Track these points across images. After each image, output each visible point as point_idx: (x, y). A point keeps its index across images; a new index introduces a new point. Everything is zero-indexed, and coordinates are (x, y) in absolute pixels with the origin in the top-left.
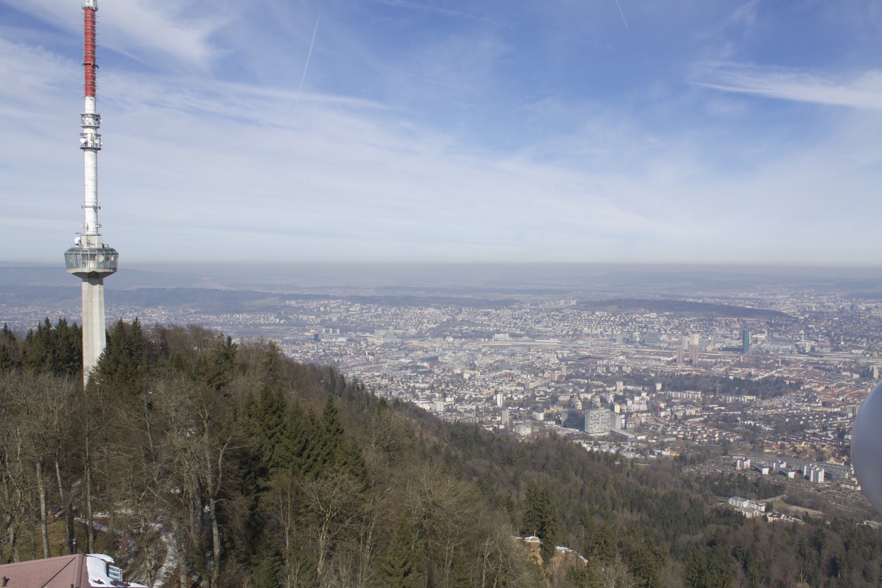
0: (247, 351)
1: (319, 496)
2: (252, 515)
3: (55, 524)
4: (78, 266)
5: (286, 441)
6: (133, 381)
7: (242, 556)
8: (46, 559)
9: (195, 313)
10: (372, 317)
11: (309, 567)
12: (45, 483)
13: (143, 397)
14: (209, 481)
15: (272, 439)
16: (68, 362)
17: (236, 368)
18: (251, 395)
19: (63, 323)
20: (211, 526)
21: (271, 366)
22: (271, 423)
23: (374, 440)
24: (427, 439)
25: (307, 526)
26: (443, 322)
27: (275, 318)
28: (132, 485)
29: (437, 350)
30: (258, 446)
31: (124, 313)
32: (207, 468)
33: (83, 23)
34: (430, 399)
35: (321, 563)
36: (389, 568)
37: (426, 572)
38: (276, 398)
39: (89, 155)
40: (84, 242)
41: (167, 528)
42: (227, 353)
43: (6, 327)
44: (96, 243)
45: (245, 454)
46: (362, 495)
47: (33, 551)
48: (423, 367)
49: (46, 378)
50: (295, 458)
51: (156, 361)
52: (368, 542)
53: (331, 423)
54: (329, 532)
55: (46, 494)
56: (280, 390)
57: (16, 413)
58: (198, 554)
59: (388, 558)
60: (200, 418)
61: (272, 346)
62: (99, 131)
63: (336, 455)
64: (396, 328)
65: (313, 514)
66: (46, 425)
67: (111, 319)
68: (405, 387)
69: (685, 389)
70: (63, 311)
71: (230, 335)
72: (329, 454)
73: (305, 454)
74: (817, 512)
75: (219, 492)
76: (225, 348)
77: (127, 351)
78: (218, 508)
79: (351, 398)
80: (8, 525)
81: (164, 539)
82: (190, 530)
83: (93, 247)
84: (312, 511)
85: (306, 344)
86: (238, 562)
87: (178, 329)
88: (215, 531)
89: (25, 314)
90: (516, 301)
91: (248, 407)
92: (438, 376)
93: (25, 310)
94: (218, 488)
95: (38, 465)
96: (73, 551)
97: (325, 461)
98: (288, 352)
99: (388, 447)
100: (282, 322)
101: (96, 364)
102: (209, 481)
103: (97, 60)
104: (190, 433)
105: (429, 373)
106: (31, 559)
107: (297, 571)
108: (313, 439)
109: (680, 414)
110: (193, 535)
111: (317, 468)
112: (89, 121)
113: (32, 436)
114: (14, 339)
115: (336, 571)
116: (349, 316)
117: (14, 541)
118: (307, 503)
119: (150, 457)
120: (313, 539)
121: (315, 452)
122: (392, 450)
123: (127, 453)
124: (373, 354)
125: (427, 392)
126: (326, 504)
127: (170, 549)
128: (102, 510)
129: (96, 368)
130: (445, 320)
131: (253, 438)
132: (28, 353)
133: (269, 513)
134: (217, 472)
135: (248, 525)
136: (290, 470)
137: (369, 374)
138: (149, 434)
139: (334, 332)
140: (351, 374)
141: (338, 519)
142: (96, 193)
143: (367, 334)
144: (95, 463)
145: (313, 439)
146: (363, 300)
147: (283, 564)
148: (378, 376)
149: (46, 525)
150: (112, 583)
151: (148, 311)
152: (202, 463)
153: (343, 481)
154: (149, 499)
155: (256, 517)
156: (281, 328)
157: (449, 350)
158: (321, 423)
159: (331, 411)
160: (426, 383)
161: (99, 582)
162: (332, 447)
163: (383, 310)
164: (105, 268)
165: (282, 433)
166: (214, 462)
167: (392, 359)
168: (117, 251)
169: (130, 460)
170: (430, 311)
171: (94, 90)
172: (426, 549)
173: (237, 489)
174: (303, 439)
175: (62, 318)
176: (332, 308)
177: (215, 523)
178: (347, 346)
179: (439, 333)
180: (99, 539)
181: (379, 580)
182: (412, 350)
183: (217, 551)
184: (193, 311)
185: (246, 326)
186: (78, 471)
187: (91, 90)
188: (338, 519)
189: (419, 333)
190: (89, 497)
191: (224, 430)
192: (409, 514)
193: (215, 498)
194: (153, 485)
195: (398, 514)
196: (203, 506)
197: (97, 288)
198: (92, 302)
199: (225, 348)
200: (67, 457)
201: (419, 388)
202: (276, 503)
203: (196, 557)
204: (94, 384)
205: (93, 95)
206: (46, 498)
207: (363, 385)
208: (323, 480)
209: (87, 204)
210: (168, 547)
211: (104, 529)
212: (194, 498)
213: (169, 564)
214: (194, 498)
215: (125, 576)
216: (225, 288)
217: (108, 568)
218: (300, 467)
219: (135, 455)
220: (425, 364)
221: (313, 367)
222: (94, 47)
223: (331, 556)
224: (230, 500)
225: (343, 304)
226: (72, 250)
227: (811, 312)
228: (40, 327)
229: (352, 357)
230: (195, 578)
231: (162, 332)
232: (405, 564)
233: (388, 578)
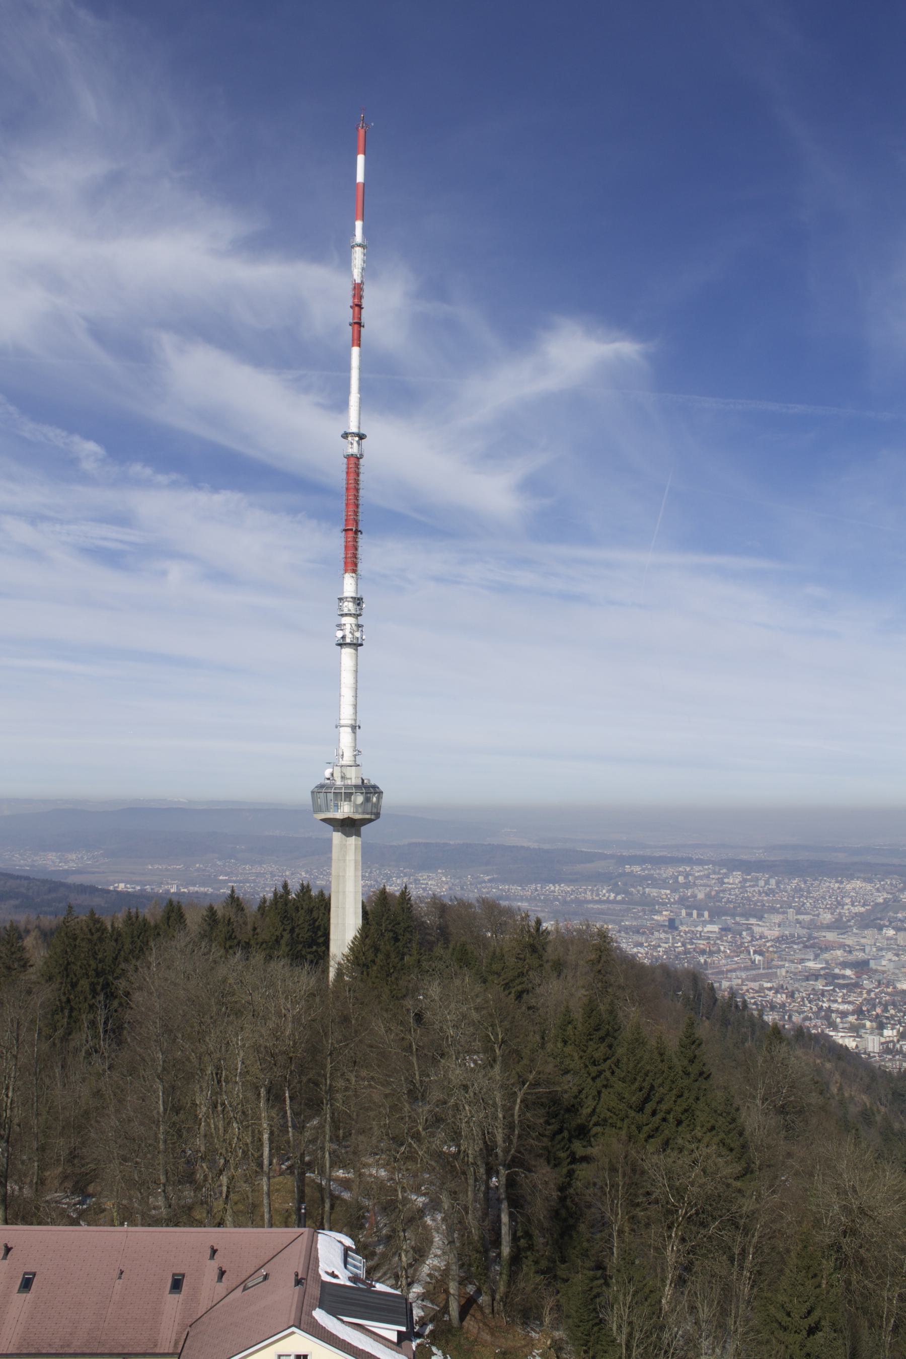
0: (565, 941)
1: (669, 1179)
2: (563, 1199)
3: (281, 1178)
4: (328, 810)
5: (619, 1086)
6: (397, 979)
7: (544, 1264)
8: (266, 1230)
9: (490, 881)
10: (760, 893)
11: (647, 1296)
12: (270, 1118)
13: (409, 1003)
14: (499, 1138)
15: (598, 1080)
16: (310, 946)
17: (547, 966)
18: (568, 1010)
19: (305, 890)
20: (500, 1210)
21: (599, 967)
22: (597, 1055)
23: (761, 1092)
24: (851, 1098)
25: (647, 1225)
26: (877, 904)
27: (609, 891)
28: (387, 1135)
29: (867, 949)
30: (575, 1090)
31: (389, 878)
32: (496, 1118)
33: (344, 476)
34: (855, 1030)
35: (668, 1290)
36: (781, 1316)
37: (847, 1333)
38: (605, 1016)
39: (347, 652)
40: (337, 776)
41: (435, 1205)
42: (535, 942)
43: (233, 891)
44: (353, 776)
45: (555, 1101)
46: (738, 1184)
47: (250, 1215)
48: (844, 977)
49: (279, 967)
50: (632, 1113)
51: (431, 950)
52: (747, 1264)
53: (692, 1061)
54: (683, 1240)
55: (272, 1133)
56: (612, 1003)
57: (238, 1013)
58: (477, 1252)
59: (781, 1298)
60: (490, 1041)
61: (603, 935)
62: (361, 620)
63: (698, 1113)
64: (798, 913)
65: (658, 1207)
66: (276, 1034)
67: (371, 886)
68: (815, 1009)
70: (307, 872)
71: (541, 915)
72: (686, 1111)
73: (649, 1107)
75: (514, 1157)
76: (531, 935)
77: (391, 934)
78: (511, 1183)
79: (725, 1022)
80: (221, 1172)
81: (428, 1220)
82: (467, 1213)
83: (349, 782)
84: (657, 1202)
85: (656, 933)
86: (537, 1272)
87: (464, 905)
88: (505, 1218)
89: (258, 875)
91: (563, 1027)
92: (869, 992)
93: (257, 869)
94: (513, 1151)
95: (263, 1091)
96: (301, 1223)
97: (679, 1123)
98: (627, 945)
99: (783, 1106)
100: (619, 898)
101: (346, 951)
102: (499, 1138)
103: (360, 524)
104: (475, 1062)
105: (853, 987)
106: (246, 1226)
107: (629, 1299)
108: (661, 1085)
110: (471, 1220)
111: (666, 1132)
112: (349, 606)
113: (256, 1048)
114: (243, 909)
115: (693, 1309)
116: (723, 891)
117: (227, 1197)
118: (649, 1188)
119: (416, 1095)
120: (657, 1249)
121: (664, 1107)
122: (789, 1112)
123: (383, 1085)
124: (761, 953)
125: (852, 1019)
126: (679, 1193)
127: (437, 1239)
128: (344, 1167)
129: (347, 957)
130: (881, 900)
131: (569, 1077)
132: (258, 930)
133: (588, 1198)
134: (511, 1127)
135: (555, 1215)
136: (624, 1132)
137: (755, 985)
138: (414, 1060)
139: (700, 915)
140: (725, 984)
141: (698, 1220)
142: (355, 706)
143: (753, 921)
144: (339, 1096)
145: (661, 1085)
146: (747, 867)
147: (607, 1284)
148: (770, 989)
149: (269, 1178)
150: (350, 1279)
151: (423, 876)
152: (490, 1110)
153: (708, 1157)
154: (410, 1157)
155: (568, 1202)
156: (618, 907)
157: (889, 949)
158: (675, 1060)
159: (692, 1042)
160: (849, 1003)
161: (333, 1275)
162: (691, 1101)
163: (778, 883)
164: (364, 813)
165: (613, 1073)
166: (508, 1110)
167: (792, 962)
168: (382, 788)
169: (386, 1096)
171: (356, 565)
172: (848, 1290)
173: (540, 1156)
174: (646, 1085)
175: (305, 883)
176: (696, 878)
177: (504, 1205)
178: (720, 939)
179: (871, 921)
180: (338, 1209)
181: (765, 1336)
182: (827, 948)
183: (506, 1250)
184: (487, 878)
185: (565, 902)
186: (314, 1105)
187: (352, 564)
188: (698, 1220)
189: (837, 920)
190: (327, 1145)
191: (525, 1061)
192: (817, 1223)
193: (508, 1167)
194: (417, 1137)
195: (800, 1223)
196: (489, 1177)
197: (352, 840)
198: (345, 860)
199: (531, 935)
200: (301, 1083)
201: (837, 1011)
202: (599, 1184)
203: (475, 1255)
204: (343, 979)
205: (354, 571)
206: (271, 1141)
207: (745, 1002)
208: (675, 1153)
209: (343, 722)
210: (435, 1234)
211: (346, 1195)
212: (475, 1164)
213: (433, 1263)
214: (475, 1164)
215: (369, 1272)
216: (534, 845)
217: (346, 1256)
218: (639, 1129)
219: (393, 1090)
220: (848, 972)
221: (665, 970)
222: (357, 506)
223: (685, 1282)
224: (530, 1171)
225: (714, 873)
226: (322, 786)
228: (275, 894)
229: (727, 957)
230: (471, 1289)
231: (441, 907)
232: (809, 1313)
233: (780, 1334)
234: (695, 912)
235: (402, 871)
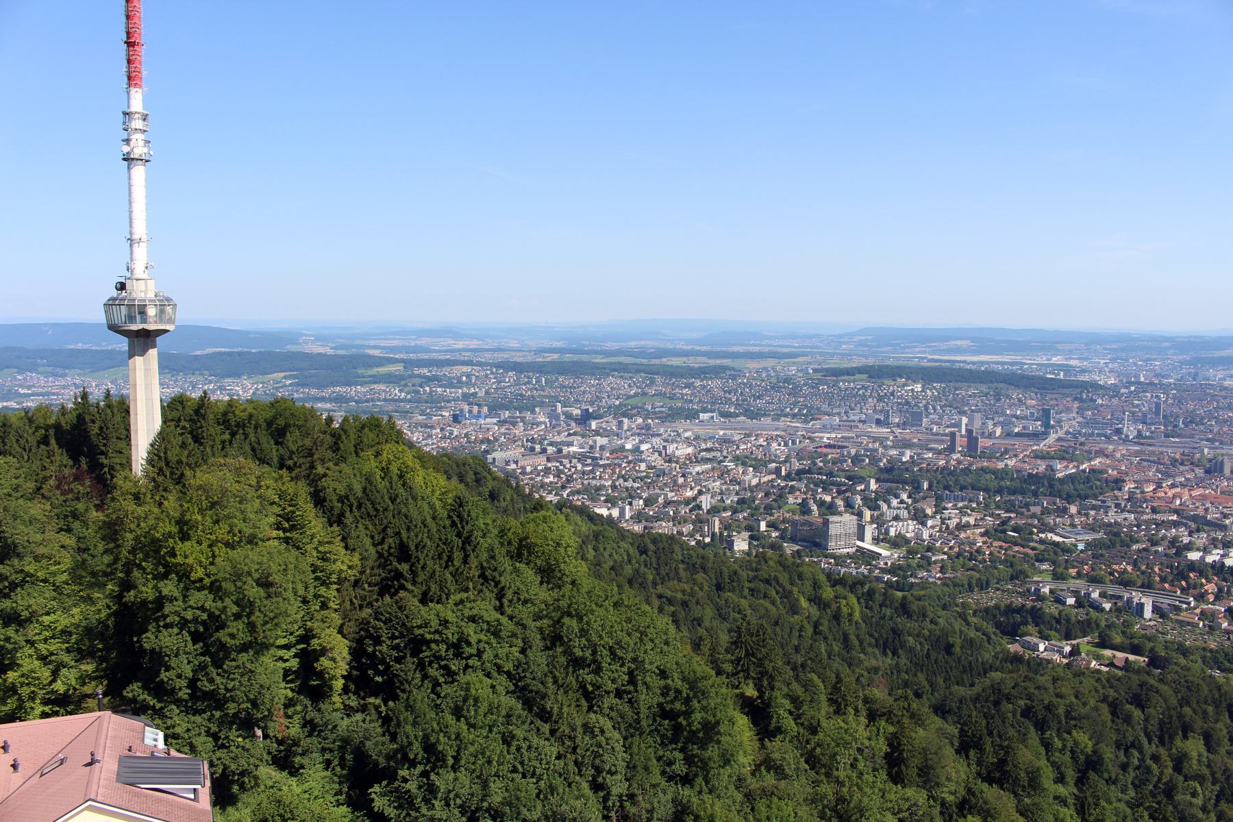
9: (291, 385)
10: (531, 390)
74: (1142, 659)
90: (728, 368)
109: (952, 523)
168: (175, 300)
227: (1139, 383)
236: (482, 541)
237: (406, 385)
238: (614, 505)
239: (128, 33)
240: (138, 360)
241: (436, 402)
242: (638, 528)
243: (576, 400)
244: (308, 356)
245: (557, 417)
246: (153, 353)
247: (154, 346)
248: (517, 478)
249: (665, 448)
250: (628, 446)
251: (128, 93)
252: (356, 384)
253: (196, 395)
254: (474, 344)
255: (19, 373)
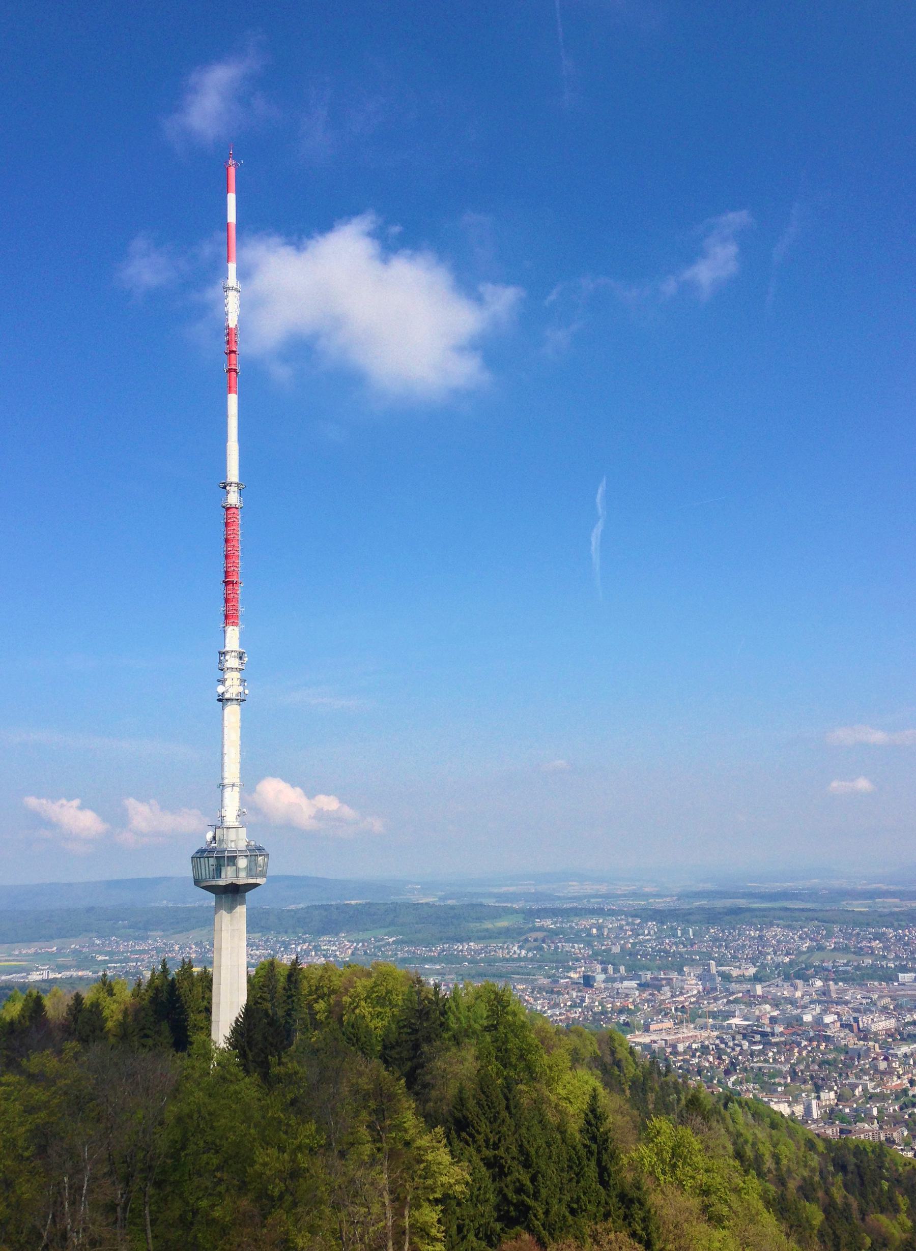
19: (187, 966)
69: (571, 909)
100: (530, 955)
139: (616, 970)
168: (268, 850)
170: (775, 933)
179: (797, 973)
234: (610, 967)
235: (300, 938)
236: (191, 1138)
237: (526, 940)
238: (796, 1100)
239: (226, 572)
240: (224, 915)
241: (564, 962)
242: (831, 1132)
243: (734, 957)
244: (417, 906)
245: (712, 978)
246: (241, 911)
247: (242, 903)
248: (666, 1059)
249: (856, 1020)
250: (808, 1018)
251: (225, 632)
252: (469, 939)
253: (286, 959)
254: (603, 889)
255: (98, 938)
